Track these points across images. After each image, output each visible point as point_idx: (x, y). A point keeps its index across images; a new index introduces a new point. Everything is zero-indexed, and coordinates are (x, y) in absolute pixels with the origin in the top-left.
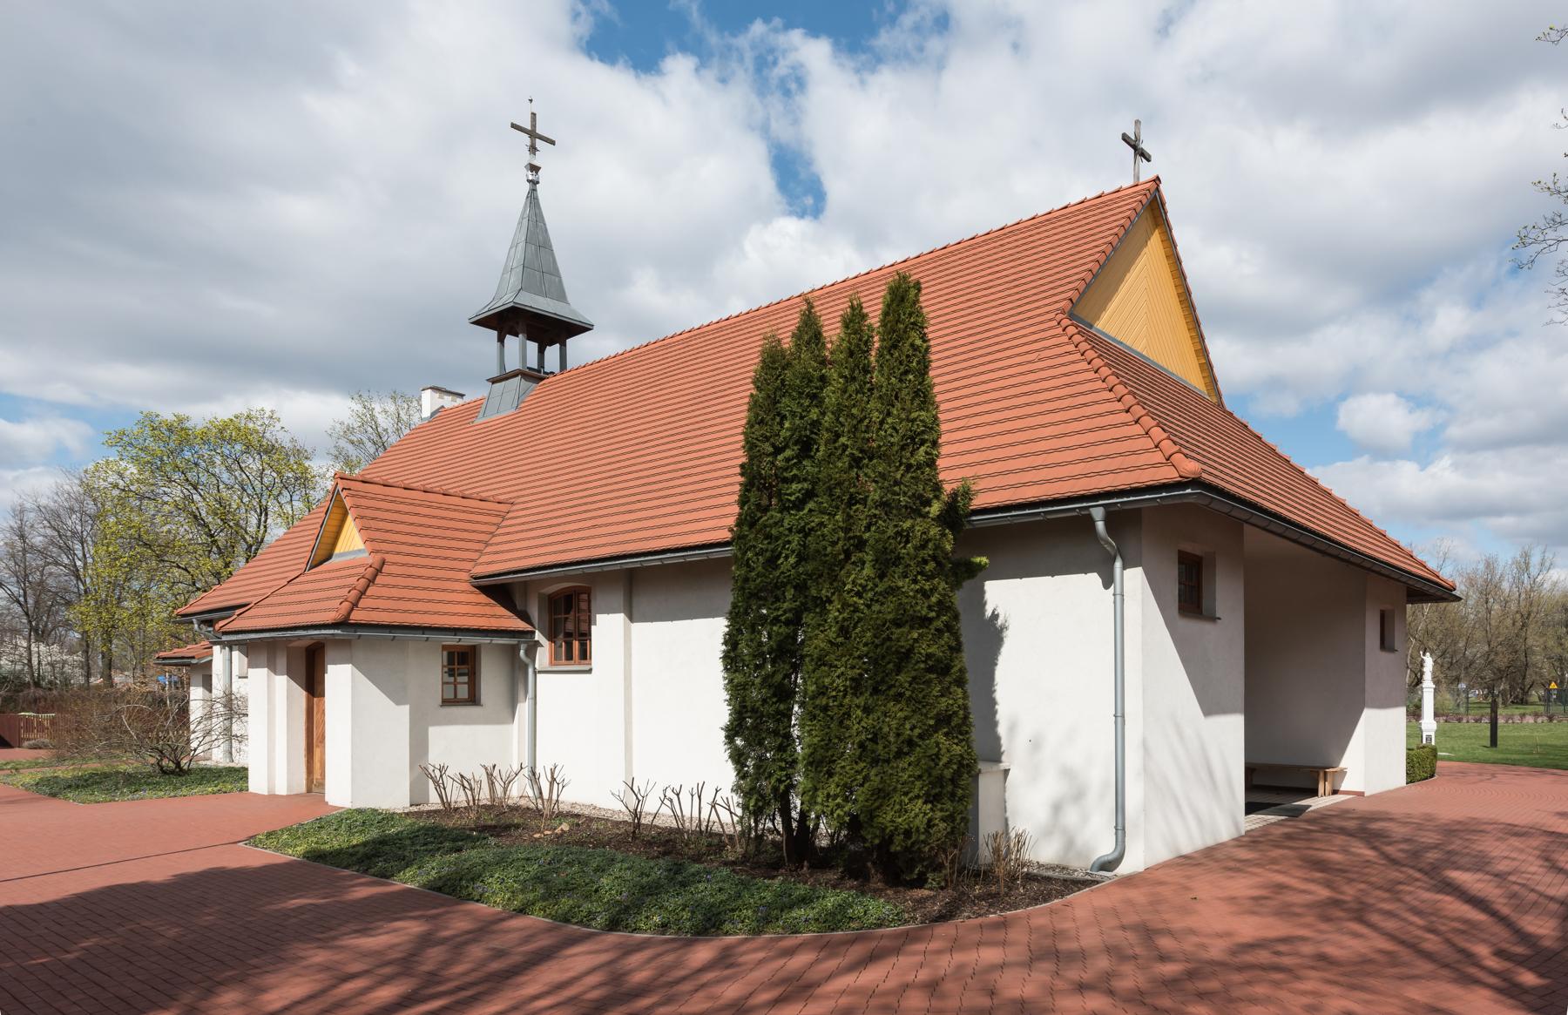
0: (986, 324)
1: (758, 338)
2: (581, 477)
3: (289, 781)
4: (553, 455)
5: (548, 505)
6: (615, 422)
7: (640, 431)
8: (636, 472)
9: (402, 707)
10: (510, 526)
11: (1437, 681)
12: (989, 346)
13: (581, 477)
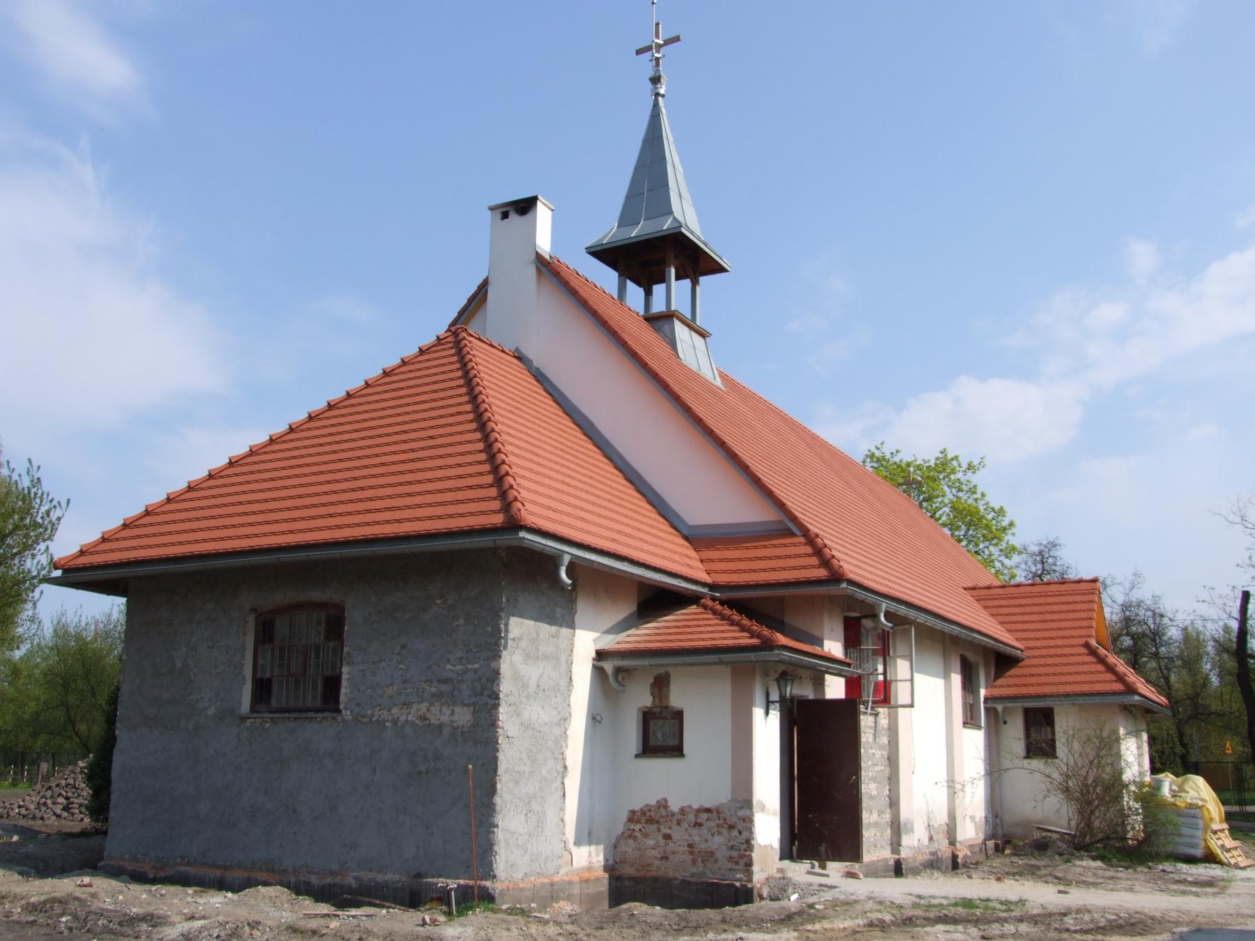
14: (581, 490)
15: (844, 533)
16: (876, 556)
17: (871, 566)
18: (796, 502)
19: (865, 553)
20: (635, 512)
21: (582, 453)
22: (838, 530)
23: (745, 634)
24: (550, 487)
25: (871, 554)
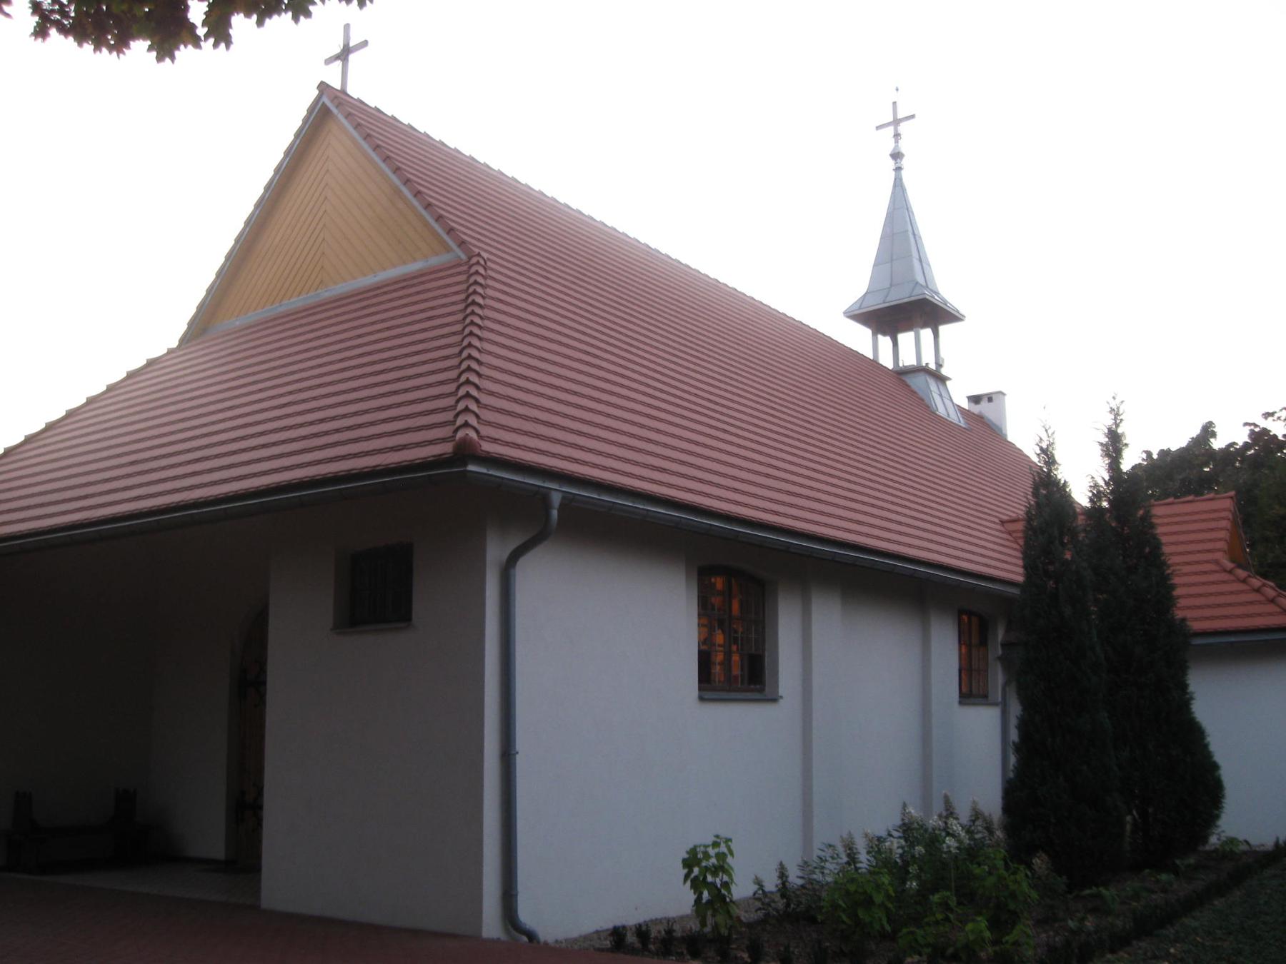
0: (602, 317)
1: (1023, 490)
2: (942, 498)
3: (988, 650)
4: (670, 343)
5: (312, 423)
6: (824, 406)
7: (383, 321)
8: (978, 493)
9: (1221, 745)
10: (446, 370)
11: (301, 140)
12: (631, 330)
13: (942, 498)
14: (949, 455)
15: (746, 387)
16: (647, 322)
17: (525, 235)
18: (557, 247)
19: (443, 162)
20: (901, 435)
21: (671, 315)
22: (900, 427)
23: (1025, 499)
24: (763, 361)
25: (967, 489)
